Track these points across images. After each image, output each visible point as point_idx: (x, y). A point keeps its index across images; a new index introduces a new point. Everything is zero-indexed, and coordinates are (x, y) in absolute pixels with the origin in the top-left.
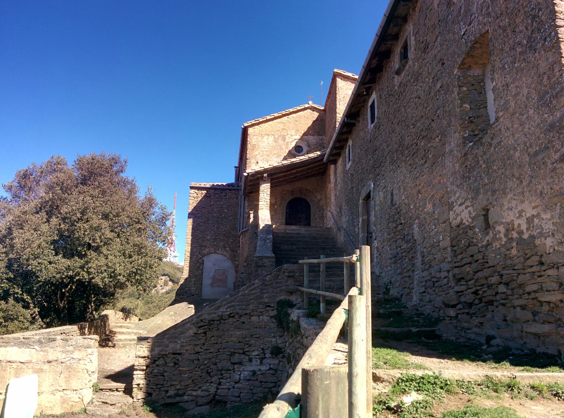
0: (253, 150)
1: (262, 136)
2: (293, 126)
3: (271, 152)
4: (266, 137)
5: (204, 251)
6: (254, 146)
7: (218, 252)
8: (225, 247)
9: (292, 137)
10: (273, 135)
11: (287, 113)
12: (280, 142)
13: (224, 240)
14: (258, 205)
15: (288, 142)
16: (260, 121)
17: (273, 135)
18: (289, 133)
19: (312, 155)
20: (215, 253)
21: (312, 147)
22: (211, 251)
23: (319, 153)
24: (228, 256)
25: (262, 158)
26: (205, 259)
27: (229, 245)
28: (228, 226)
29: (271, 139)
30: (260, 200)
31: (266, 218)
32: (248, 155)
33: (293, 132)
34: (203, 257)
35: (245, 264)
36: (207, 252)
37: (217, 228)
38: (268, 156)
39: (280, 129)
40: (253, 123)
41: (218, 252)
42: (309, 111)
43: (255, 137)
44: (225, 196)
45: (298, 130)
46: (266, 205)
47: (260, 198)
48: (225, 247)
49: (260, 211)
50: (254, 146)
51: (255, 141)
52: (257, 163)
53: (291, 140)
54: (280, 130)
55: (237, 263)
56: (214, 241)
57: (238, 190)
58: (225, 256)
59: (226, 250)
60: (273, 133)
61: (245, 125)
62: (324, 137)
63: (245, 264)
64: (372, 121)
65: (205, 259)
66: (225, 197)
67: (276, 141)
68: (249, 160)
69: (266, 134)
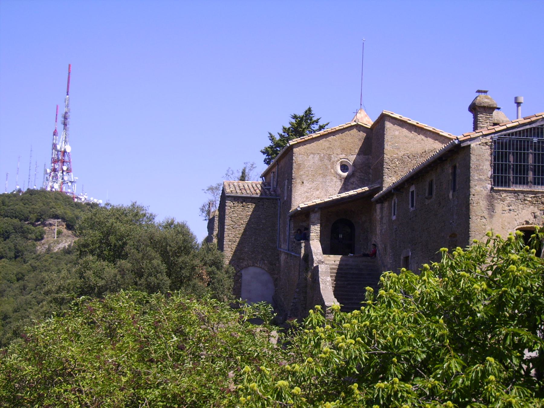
0: (298, 169)
1: (308, 156)
2: (339, 144)
3: (316, 172)
4: (312, 155)
5: (242, 264)
6: (299, 165)
7: (256, 265)
8: (264, 260)
9: (338, 156)
10: (319, 154)
11: (333, 130)
12: (326, 162)
13: (263, 253)
14: (309, 236)
15: (334, 161)
16: (306, 139)
17: (319, 154)
18: (335, 152)
19: (359, 190)
20: (253, 266)
21: (358, 167)
22: (249, 265)
23: (366, 188)
24: (266, 269)
25: (308, 178)
26: (243, 272)
27: (267, 258)
28: (266, 238)
29: (317, 157)
30: (311, 231)
31: (318, 251)
32: (293, 175)
33: (339, 151)
34: (241, 269)
35: (297, 290)
36: (245, 265)
37: (255, 239)
38: (314, 176)
39: (326, 147)
40: (298, 141)
41: (256, 265)
42: (355, 130)
43: (301, 156)
44: (263, 205)
45: (344, 149)
46: (317, 237)
47: (311, 229)
48: (264, 260)
49: (311, 242)
50: (299, 165)
51: (301, 160)
52: (303, 183)
53: (336, 159)
54: (326, 149)
55: (276, 276)
56: (252, 254)
57: (277, 199)
58: (264, 269)
59: (265, 263)
60: (318, 152)
61: (291, 144)
62: (370, 157)
63: (297, 290)
64: (412, 206)
65: (243, 272)
66: (262, 207)
67: (321, 160)
68: (294, 180)
69: (312, 153)
